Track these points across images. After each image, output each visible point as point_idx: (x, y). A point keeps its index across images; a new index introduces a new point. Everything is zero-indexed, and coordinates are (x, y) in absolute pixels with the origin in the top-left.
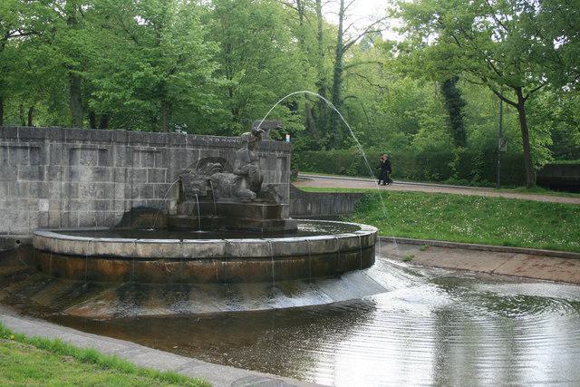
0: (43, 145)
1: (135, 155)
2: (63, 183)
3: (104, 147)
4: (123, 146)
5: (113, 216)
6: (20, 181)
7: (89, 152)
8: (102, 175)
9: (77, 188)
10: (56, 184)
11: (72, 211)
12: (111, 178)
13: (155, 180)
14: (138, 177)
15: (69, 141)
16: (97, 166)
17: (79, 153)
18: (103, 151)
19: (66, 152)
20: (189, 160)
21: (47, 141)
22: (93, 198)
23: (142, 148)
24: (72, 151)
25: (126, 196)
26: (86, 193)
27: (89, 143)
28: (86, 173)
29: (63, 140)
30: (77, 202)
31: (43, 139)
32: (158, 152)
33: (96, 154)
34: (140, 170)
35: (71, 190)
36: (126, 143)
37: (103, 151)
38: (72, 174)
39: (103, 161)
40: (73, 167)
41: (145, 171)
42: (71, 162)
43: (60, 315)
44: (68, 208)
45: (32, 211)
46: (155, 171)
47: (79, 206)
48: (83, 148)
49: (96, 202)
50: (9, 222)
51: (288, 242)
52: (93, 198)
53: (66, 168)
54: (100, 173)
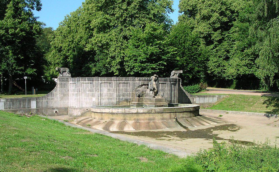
6: (88, 92)
16: (109, 88)
22: (107, 97)
41: (123, 89)
46: (126, 89)
53: (99, 88)
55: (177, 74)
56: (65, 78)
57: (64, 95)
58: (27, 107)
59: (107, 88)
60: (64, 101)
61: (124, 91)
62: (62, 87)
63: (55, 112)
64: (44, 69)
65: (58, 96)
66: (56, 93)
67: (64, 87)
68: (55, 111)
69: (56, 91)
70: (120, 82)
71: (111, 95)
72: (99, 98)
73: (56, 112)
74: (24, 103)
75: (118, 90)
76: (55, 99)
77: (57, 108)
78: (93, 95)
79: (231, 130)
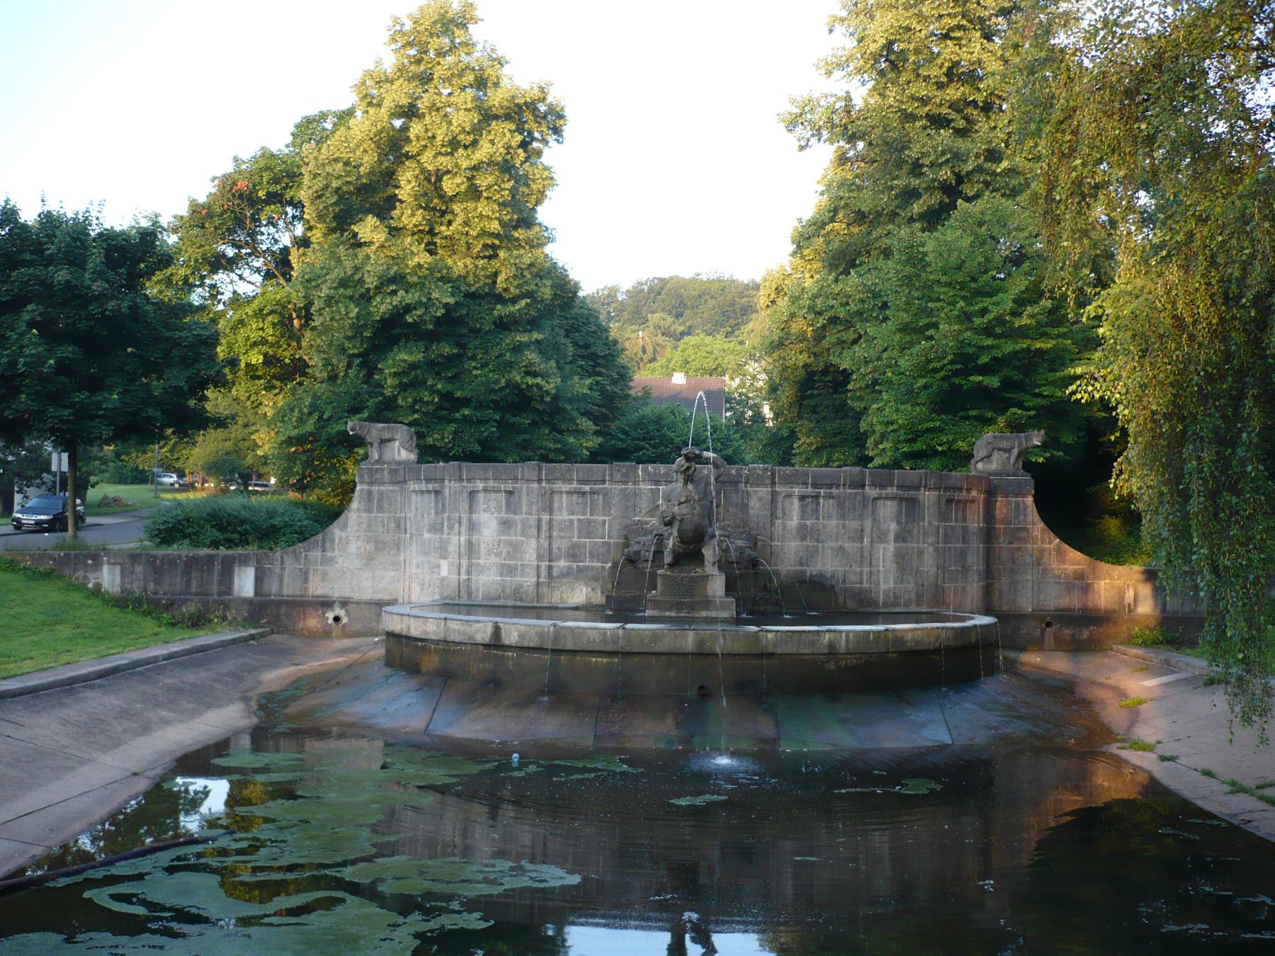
0: (443, 487)
1: (556, 498)
2: (462, 539)
3: (510, 486)
4: (535, 485)
5: (522, 586)
6: (426, 536)
7: (493, 495)
8: (510, 527)
9: (479, 545)
10: (455, 539)
11: (473, 577)
12: (519, 532)
13: (589, 535)
14: (561, 530)
15: (469, 480)
16: (503, 515)
17: (481, 496)
18: (510, 493)
19: (465, 495)
20: (644, 505)
21: (446, 482)
22: (498, 560)
23: (566, 487)
24: (472, 494)
25: (539, 558)
26: (489, 552)
27: (491, 483)
28: (489, 522)
29: (461, 479)
30: (479, 565)
31: (443, 480)
32: (593, 493)
33: (502, 497)
34: (564, 521)
35: (471, 548)
36: (539, 481)
37: (510, 493)
38: (472, 527)
39: (512, 507)
40: (329, 554)
41: (571, 521)
42: (471, 510)
43: (527, 773)
44: (468, 573)
45: (435, 576)
46: (589, 522)
47: (481, 570)
48: (485, 490)
49: (503, 565)
50: (1174, 661)
51: (643, 630)
52: (498, 560)
53: (465, 516)
54: (506, 525)
55: (1008, 451)
56: (383, 470)
57: (380, 546)
58: (214, 588)
59: (495, 515)
60: (377, 573)
61: (579, 533)
62: (368, 510)
63: (330, 621)
64: (1039, 431)
65: (352, 548)
66: (344, 535)
67: (380, 509)
68: (330, 616)
69: (345, 527)
70: (559, 485)
71: (515, 549)
72: (464, 562)
73: (337, 619)
74: (205, 574)
75: (545, 527)
76: (341, 563)
77: (344, 603)
78: (443, 552)
79: (1223, 820)
